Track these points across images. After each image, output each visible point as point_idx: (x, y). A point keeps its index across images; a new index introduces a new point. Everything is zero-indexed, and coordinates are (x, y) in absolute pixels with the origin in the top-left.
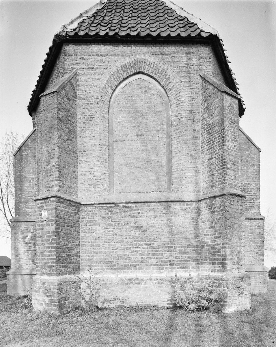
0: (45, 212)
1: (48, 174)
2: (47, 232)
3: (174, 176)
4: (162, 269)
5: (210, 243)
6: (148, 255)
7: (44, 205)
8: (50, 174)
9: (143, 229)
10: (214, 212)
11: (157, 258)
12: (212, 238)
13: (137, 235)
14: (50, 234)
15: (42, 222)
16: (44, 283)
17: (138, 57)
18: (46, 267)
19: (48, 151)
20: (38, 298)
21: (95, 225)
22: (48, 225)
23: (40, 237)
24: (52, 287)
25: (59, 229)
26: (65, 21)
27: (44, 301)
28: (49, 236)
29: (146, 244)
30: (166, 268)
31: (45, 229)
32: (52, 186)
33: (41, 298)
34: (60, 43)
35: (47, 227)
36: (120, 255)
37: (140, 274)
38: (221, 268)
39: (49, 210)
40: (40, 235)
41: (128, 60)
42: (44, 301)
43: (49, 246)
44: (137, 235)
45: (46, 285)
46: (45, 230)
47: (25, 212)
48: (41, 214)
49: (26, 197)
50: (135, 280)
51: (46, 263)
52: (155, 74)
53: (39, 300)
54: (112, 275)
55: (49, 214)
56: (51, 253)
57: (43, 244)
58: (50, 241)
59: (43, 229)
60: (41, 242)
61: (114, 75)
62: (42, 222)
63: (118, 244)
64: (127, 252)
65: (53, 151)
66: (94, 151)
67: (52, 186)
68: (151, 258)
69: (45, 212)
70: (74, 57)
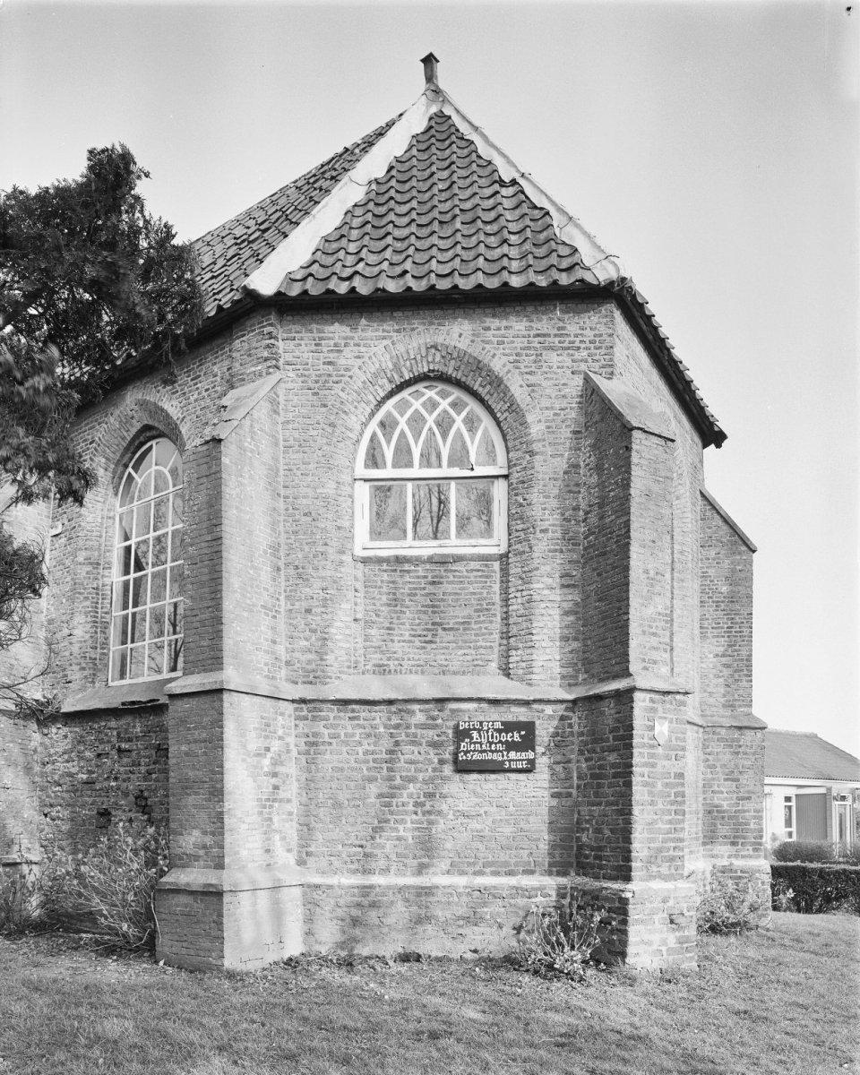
0: (661, 725)
1: (646, 628)
2: (663, 773)
5: (725, 807)
7: (659, 707)
8: (651, 630)
10: (738, 753)
12: (731, 799)
14: (672, 780)
15: (652, 747)
16: (664, 901)
18: (659, 860)
19: (646, 572)
20: (646, 937)
22: (668, 758)
23: (646, 784)
24: (685, 905)
27: (664, 942)
28: (671, 783)
31: (659, 766)
32: (655, 662)
33: (656, 938)
35: (666, 763)
38: (751, 853)
39: (671, 722)
40: (646, 778)
42: (664, 942)
43: (669, 807)
45: (671, 903)
46: (659, 769)
47: (252, 661)
48: (652, 728)
49: (253, 605)
51: (660, 850)
52: (480, 385)
53: (649, 943)
55: (671, 732)
56: (673, 826)
57: (652, 803)
58: (673, 798)
59: (653, 765)
60: (647, 798)
62: (652, 747)
65: (659, 577)
67: (655, 662)
69: (661, 725)
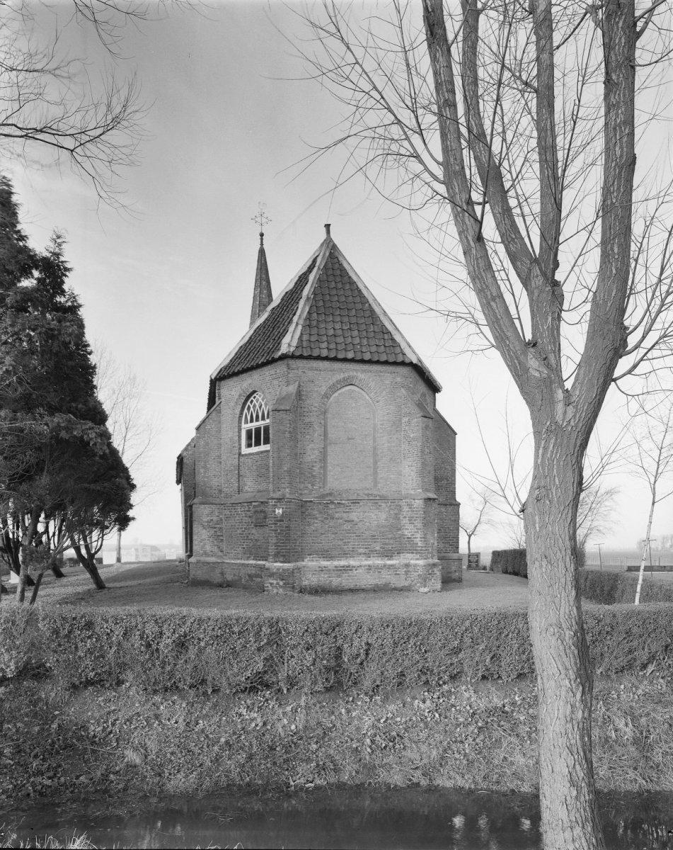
3: (380, 476)
4: (370, 557)
6: (358, 545)
9: (354, 523)
11: (366, 548)
13: (349, 527)
17: (351, 373)
21: (313, 519)
25: (642, 600)
26: (212, 369)
29: (356, 536)
30: (373, 557)
34: (214, 383)
36: (334, 545)
37: (352, 562)
39: (283, 508)
41: (342, 376)
44: (349, 527)
48: (275, 512)
50: (347, 567)
54: (328, 563)
61: (330, 388)
63: (333, 536)
64: (340, 543)
66: (313, 454)
68: (360, 548)
70: (296, 371)
